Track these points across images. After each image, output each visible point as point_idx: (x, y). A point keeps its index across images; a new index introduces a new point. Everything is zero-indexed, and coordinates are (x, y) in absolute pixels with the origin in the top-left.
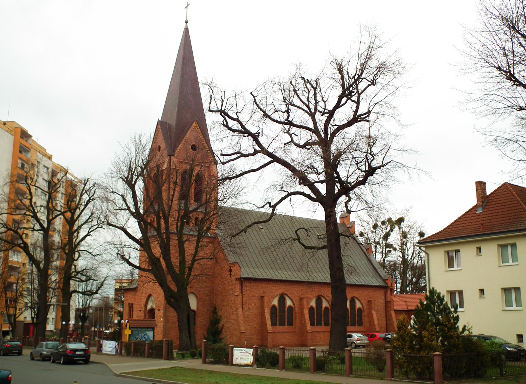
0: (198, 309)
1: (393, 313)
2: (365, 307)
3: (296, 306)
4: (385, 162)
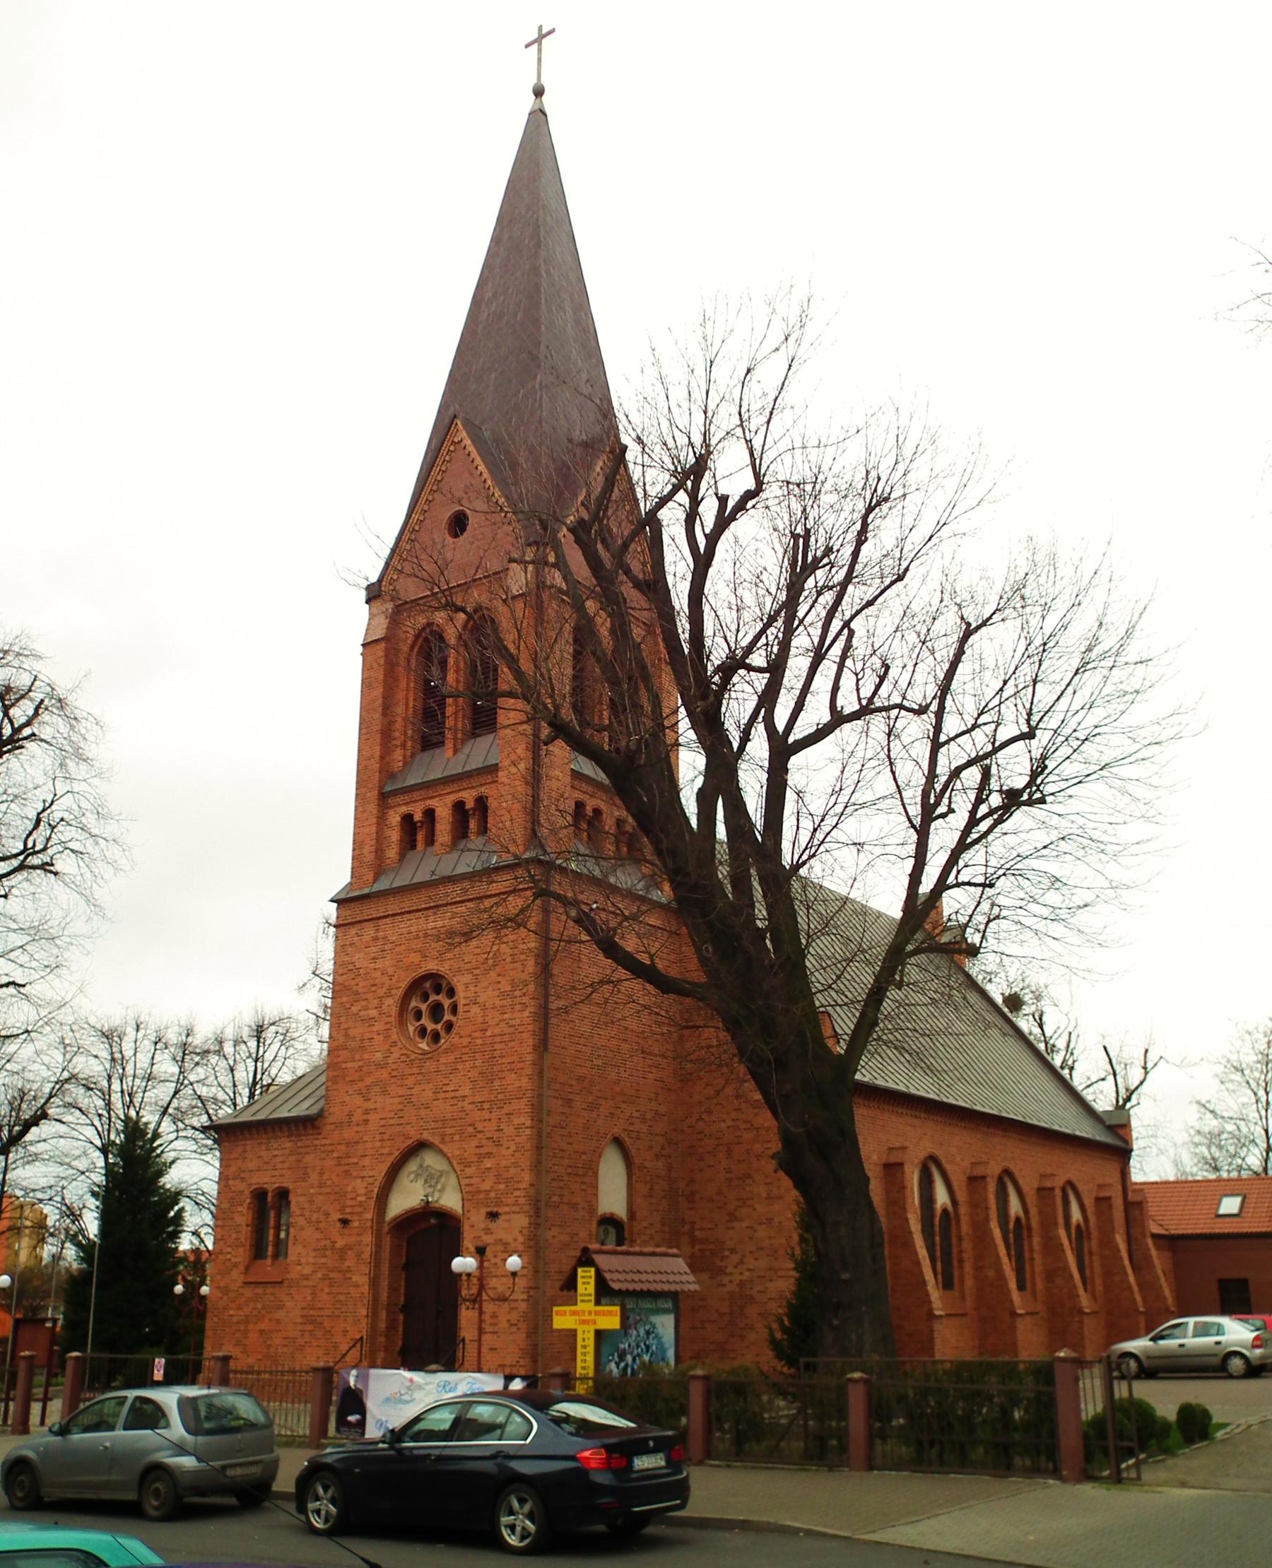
0: (632, 1214)
1: (1150, 1241)
2: (1092, 1220)
3: (963, 1210)
4: (1028, 706)
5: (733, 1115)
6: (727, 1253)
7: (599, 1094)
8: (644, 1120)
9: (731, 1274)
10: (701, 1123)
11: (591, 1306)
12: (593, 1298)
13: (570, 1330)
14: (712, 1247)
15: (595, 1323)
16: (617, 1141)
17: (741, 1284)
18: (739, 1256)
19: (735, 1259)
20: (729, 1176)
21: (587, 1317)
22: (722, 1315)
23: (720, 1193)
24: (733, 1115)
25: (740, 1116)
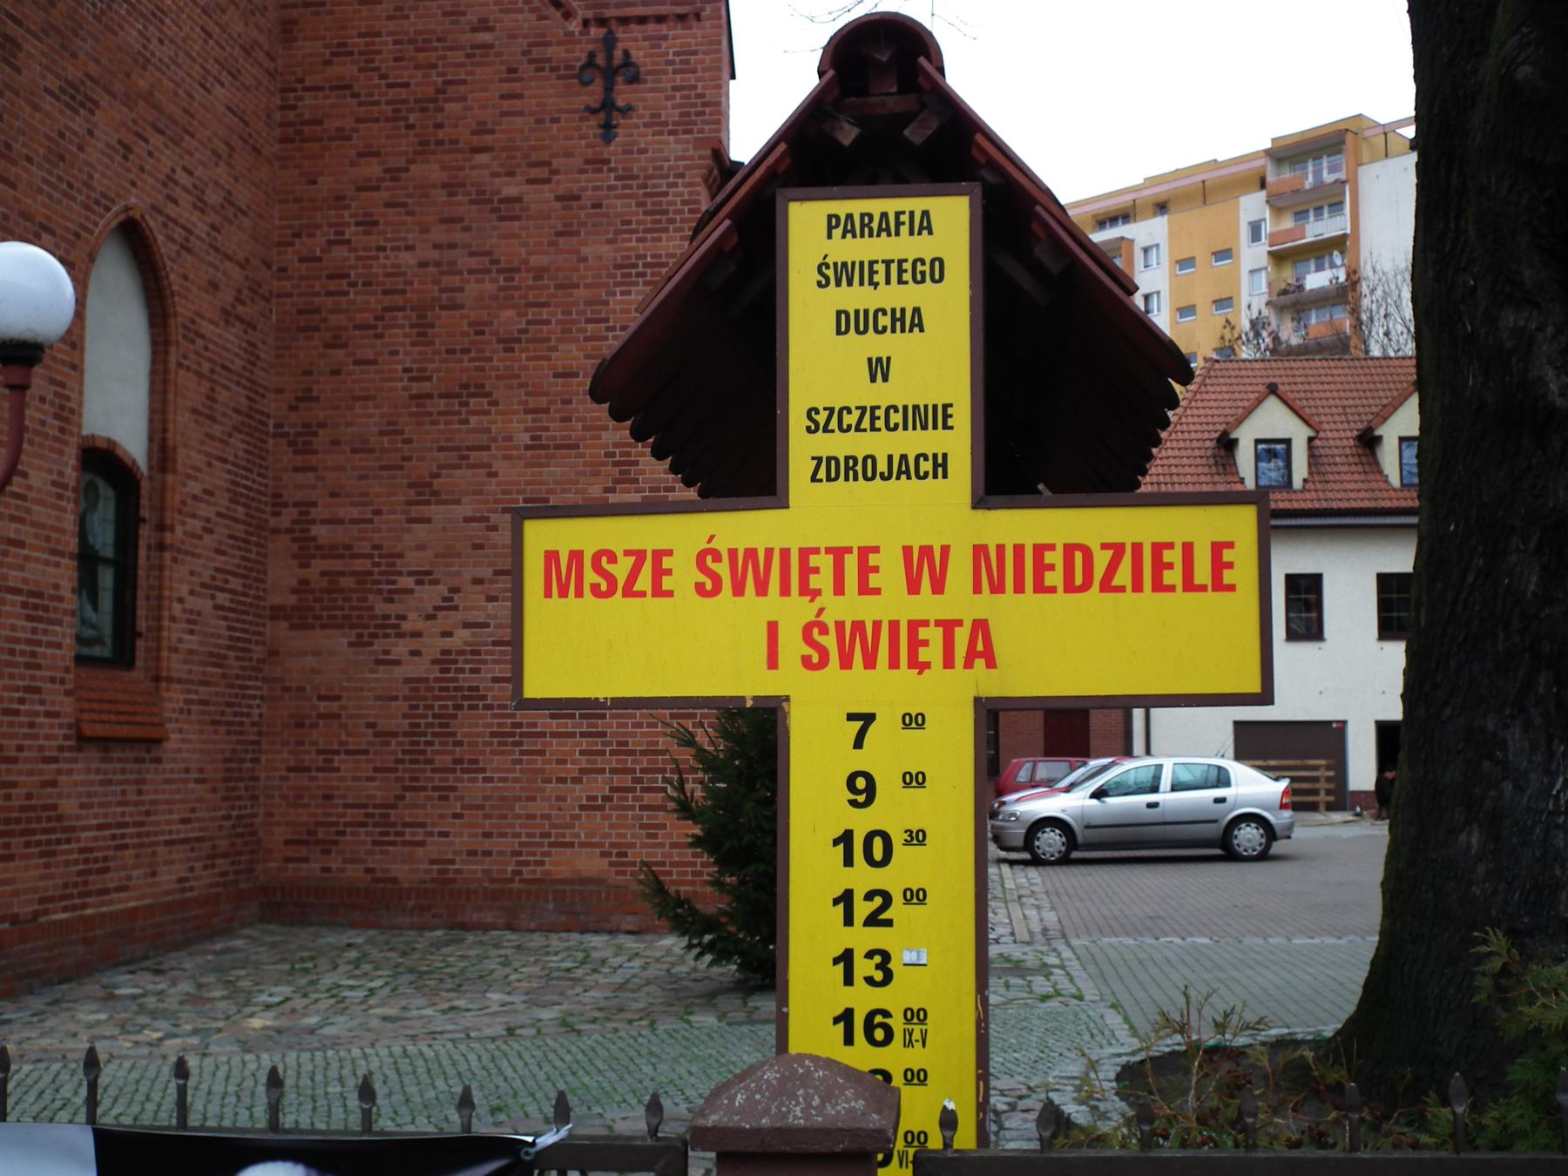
5: (438, 234)
6: (408, 582)
7: (93, 68)
8: (201, 205)
9: (417, 634)
10: (339, 252)
11: (946, 512)
12: (958, 442)
13: (730, 711)
14: (361, 565)
15: (983, 649)
16: (133, 236)
17: (445, 660)
18: (442, 589)
19: (430, 596)
20: (416, 388)
21: (893, 603)
22: (385, 735)
23: (391, 430)
24: (438, 234)
25: (459, 237)
